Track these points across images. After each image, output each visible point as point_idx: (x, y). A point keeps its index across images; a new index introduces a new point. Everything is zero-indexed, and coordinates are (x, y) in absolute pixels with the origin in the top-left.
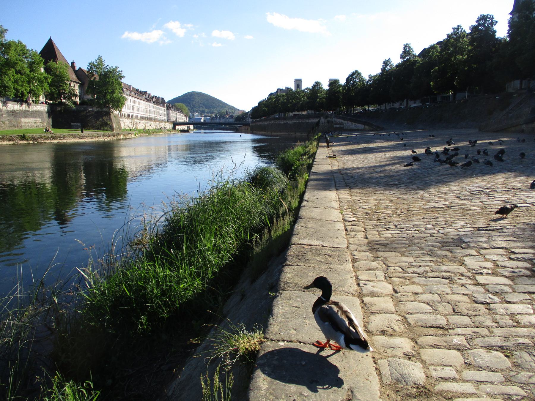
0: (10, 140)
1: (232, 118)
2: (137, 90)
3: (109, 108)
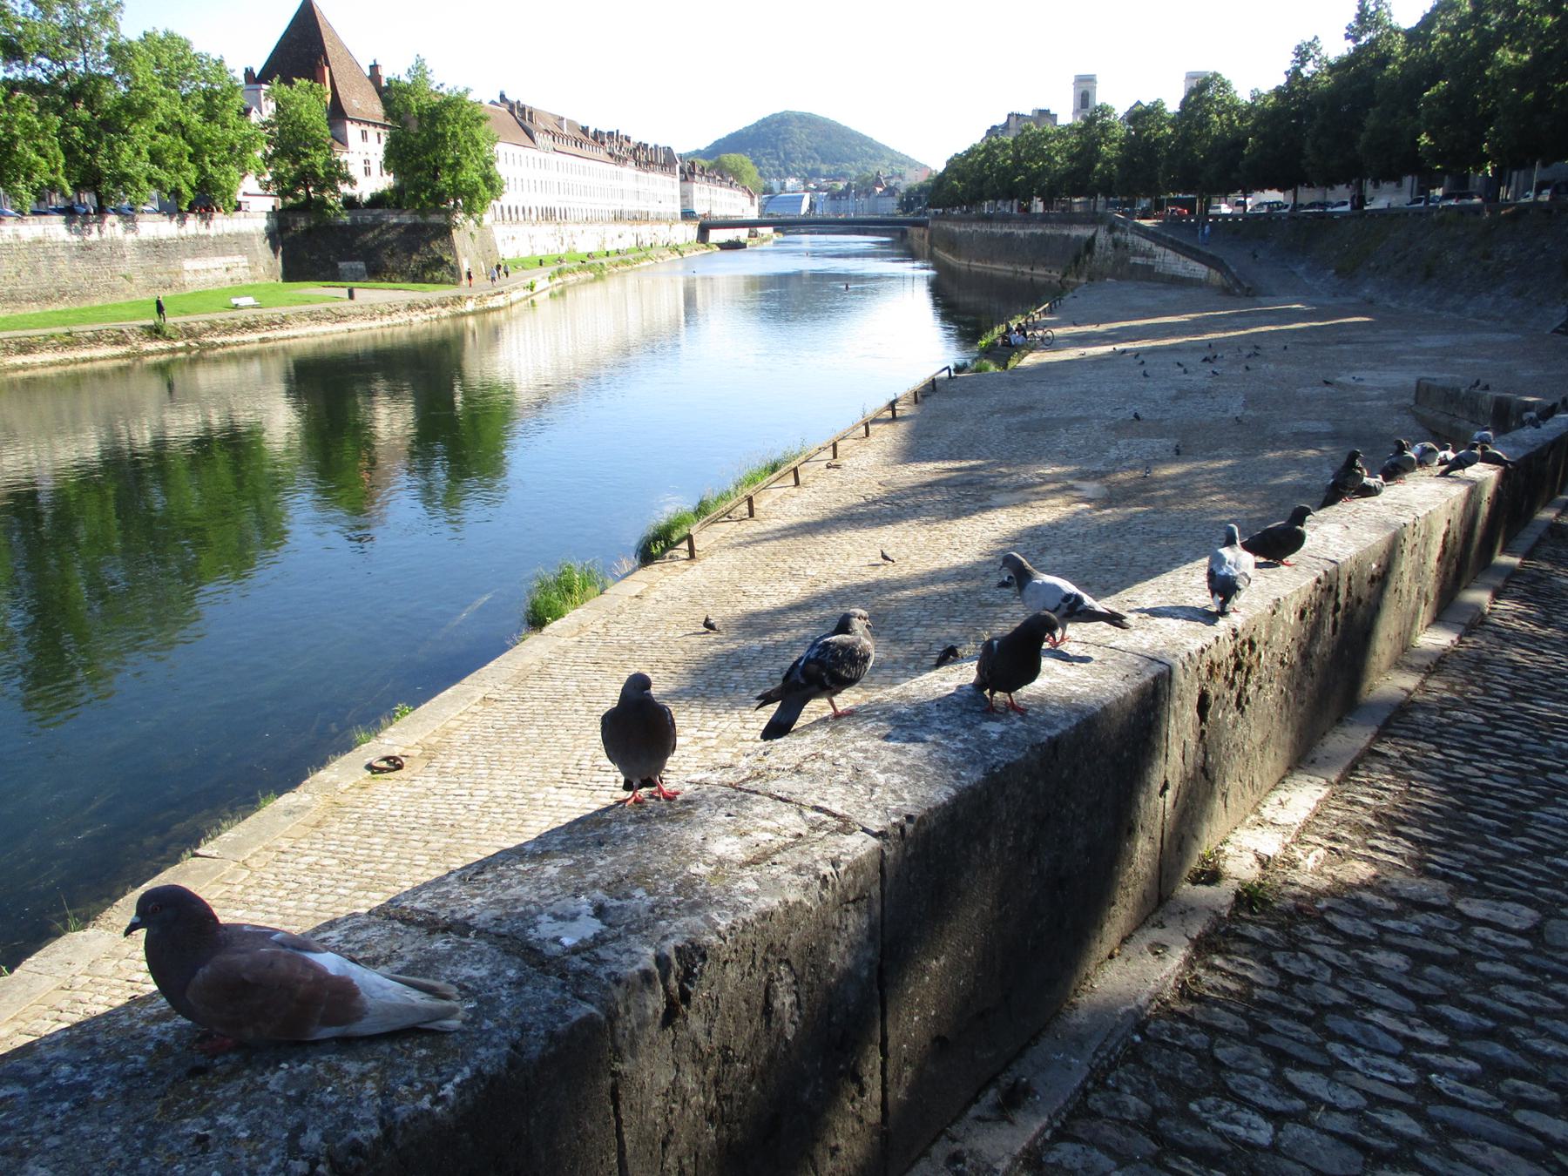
0: (117, 343)
1: (893, 195)
2: (585, 130)
3: (449, 213)
